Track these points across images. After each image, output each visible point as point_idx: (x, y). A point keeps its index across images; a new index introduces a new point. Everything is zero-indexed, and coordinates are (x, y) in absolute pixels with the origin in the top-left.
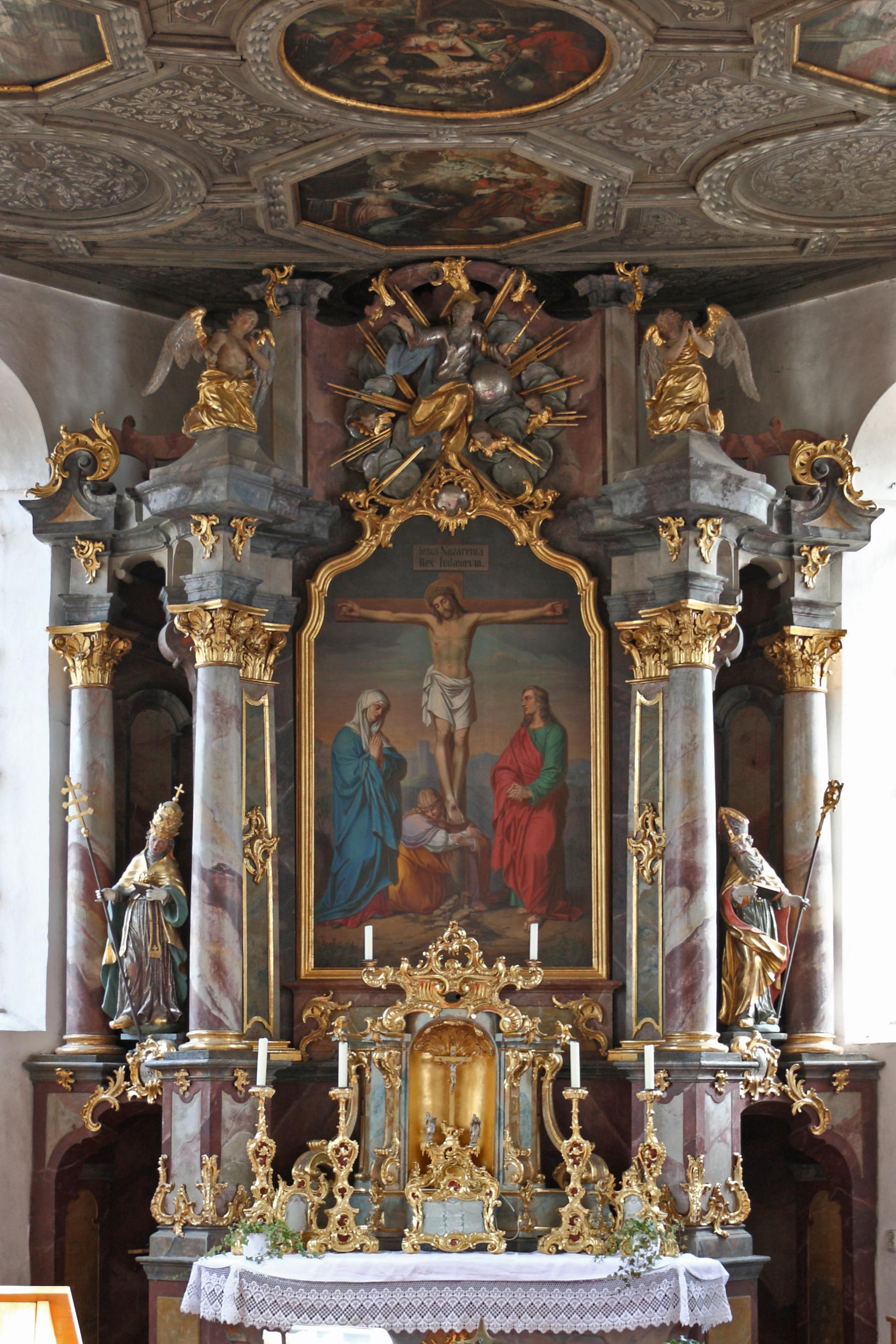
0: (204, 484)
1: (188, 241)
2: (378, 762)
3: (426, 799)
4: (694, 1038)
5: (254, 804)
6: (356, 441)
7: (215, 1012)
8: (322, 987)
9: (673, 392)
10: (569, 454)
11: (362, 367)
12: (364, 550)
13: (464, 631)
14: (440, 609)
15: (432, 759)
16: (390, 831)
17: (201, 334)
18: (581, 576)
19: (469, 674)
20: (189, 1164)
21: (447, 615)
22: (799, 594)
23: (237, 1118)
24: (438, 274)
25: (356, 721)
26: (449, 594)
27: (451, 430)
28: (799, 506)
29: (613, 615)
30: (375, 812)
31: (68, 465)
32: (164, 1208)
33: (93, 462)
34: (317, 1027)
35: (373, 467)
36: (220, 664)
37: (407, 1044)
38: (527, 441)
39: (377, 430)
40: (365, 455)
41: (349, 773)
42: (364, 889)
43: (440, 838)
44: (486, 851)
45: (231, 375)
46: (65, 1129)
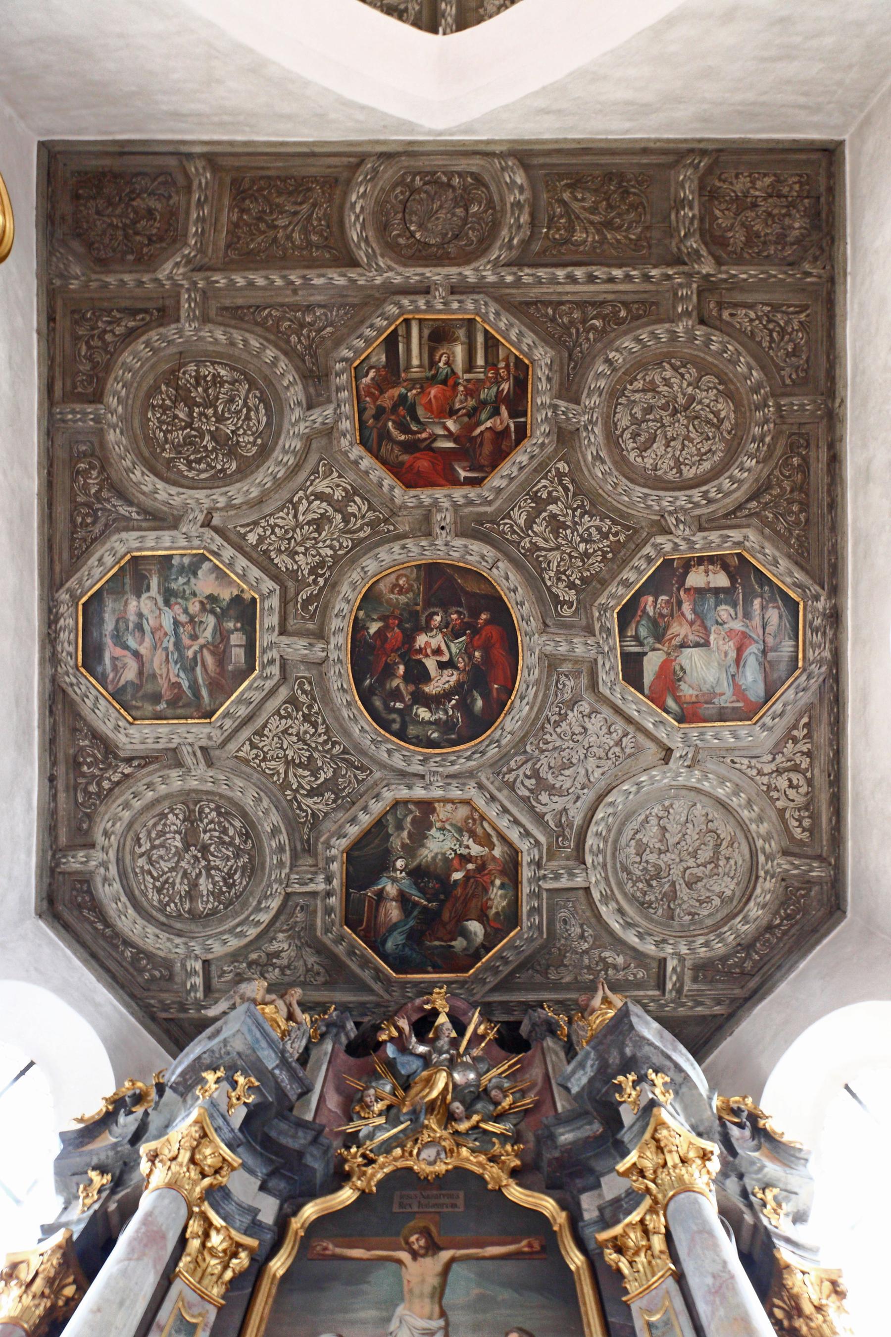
13: (439, 1268)
26: (425, 1232)
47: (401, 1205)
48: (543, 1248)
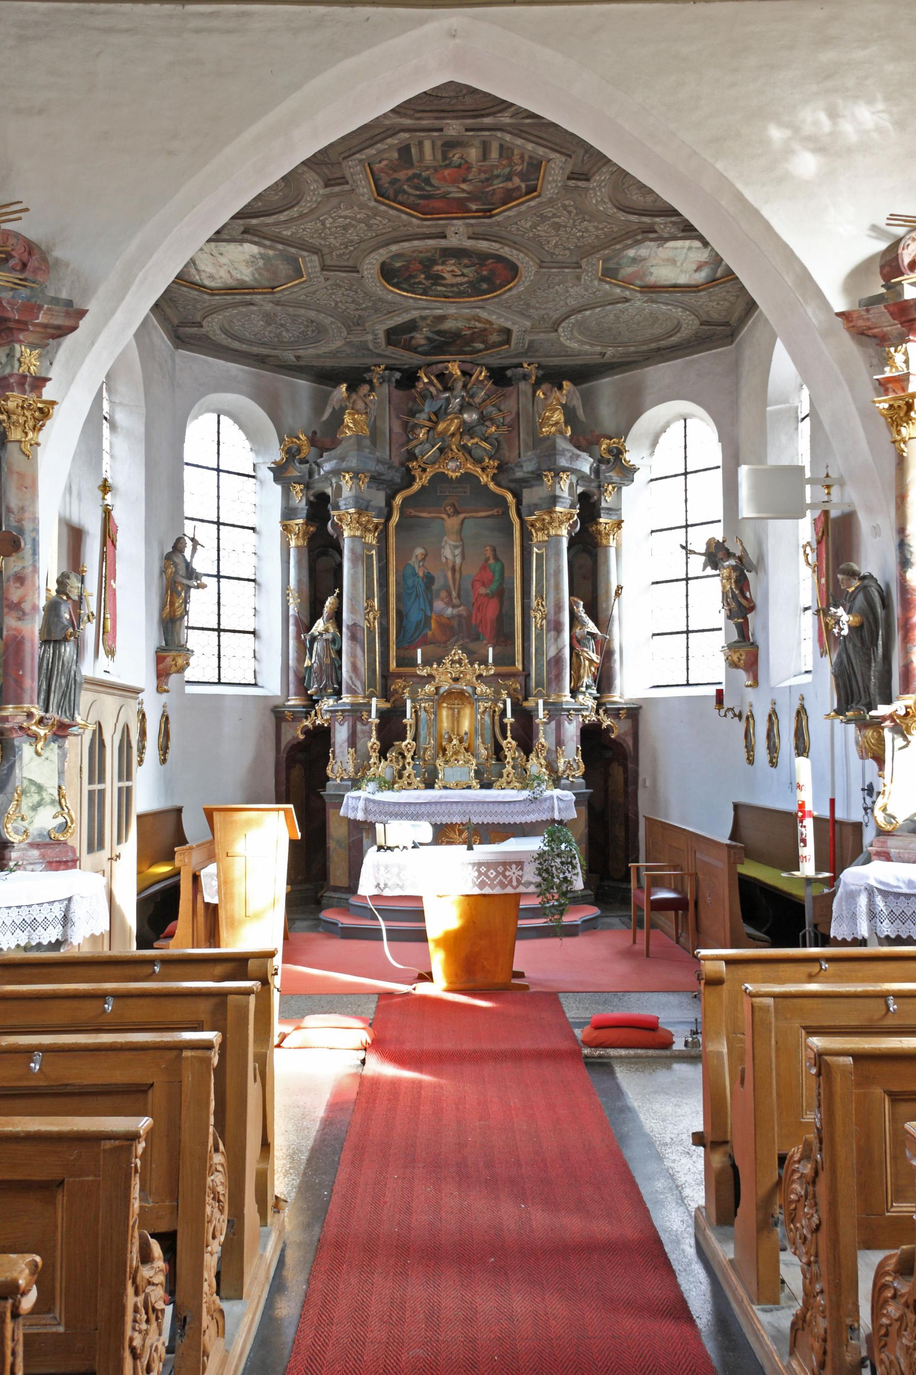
2: (423, 578)
3: (443, 594)
4: (560, 696)
5: (370, 597)
6: (412, 440)
8: (399, 676)
9: (549, 418)
10: (504, 445)
12: (416, 487)
13: (459, 522)
15: (446, 577)
16: (428, 608)
18: (510, 497)
22: (603, 505)
23: (363, 732)
24: (447, 368)
25: (413, 561)
26: (453, 505)
27: (453, 435)
28: (603, 467)
29: (523, 514)
30: (422, 600)
31: (288, 452)
33: (299, 450)
34: (397, 693)
36: (354, 536)
38: (486, 440)
40: (416, 446)
41: (410, 582)
43: (449, 611)
44: (469, 616)
45: (358, 412)
46: (289, 737)
47: (441, 492)
48: (503, 512)
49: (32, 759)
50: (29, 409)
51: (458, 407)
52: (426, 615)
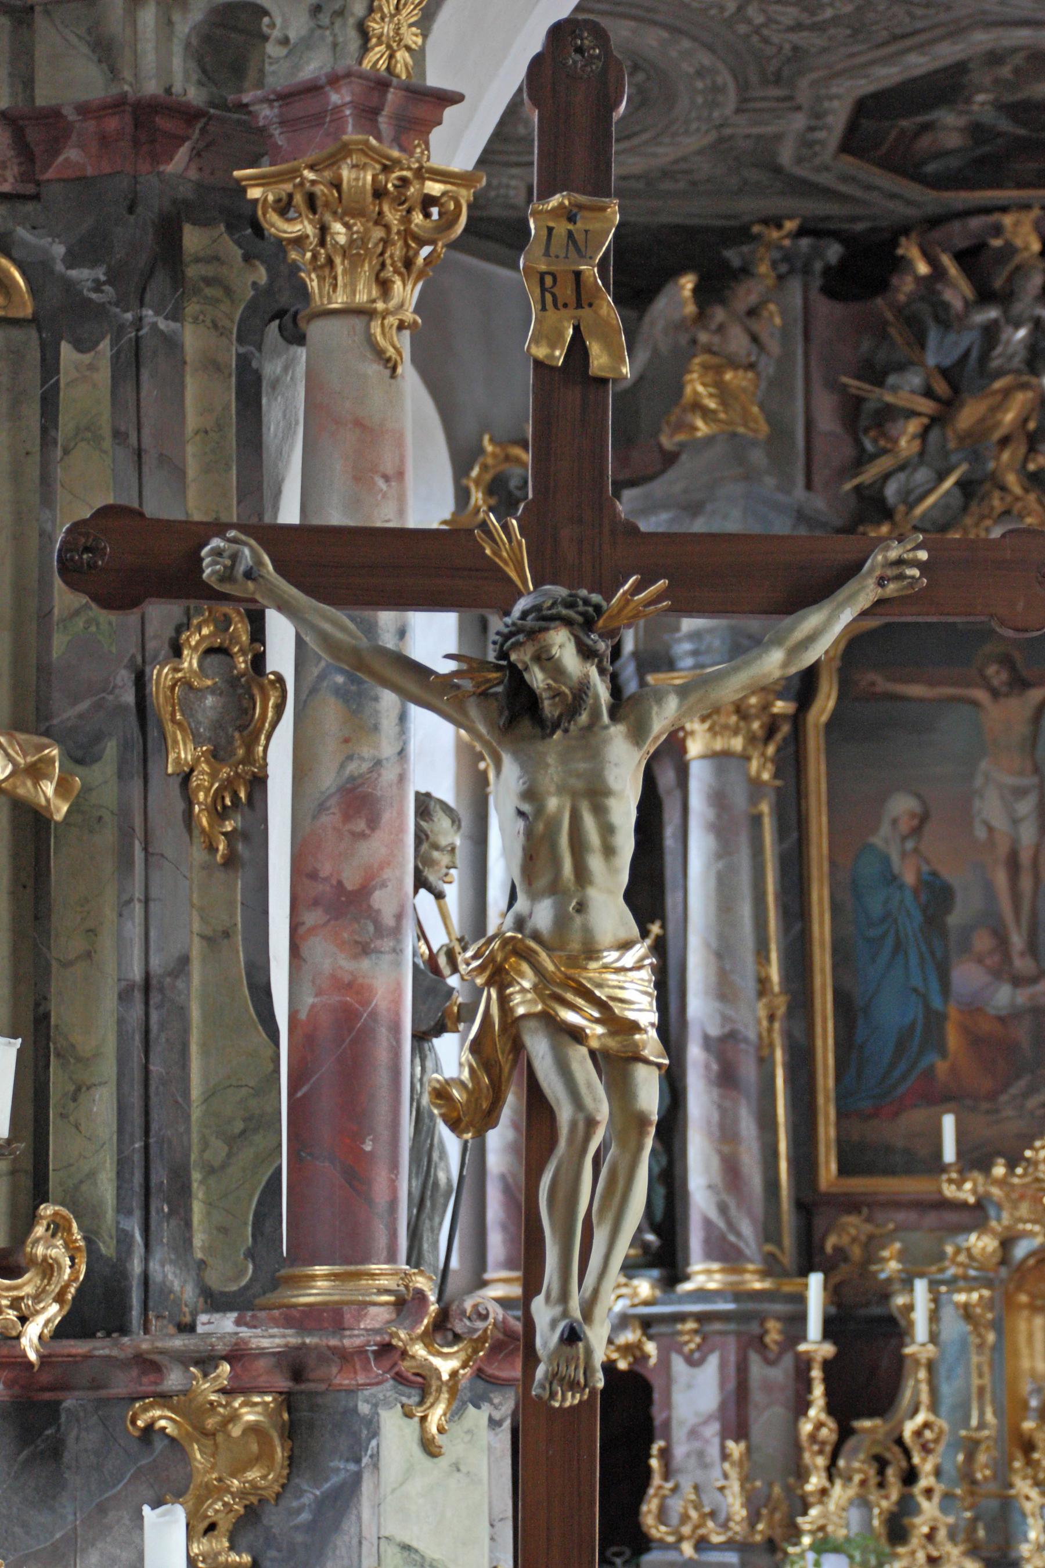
0: (709, 507)
1: (667, 185)
2: (916, 892)
3: (982, 942)
6: (873, 457)
7: (732, 1238)
8: (852, 1204)
11: (882, 356)
13: (1028, 712)
14: (995, 682)
15: (989, 887)
16: (934, 985)
17: (691, 309)
19: (1036, 770)
20: (701, 1454)
21: (1004, 689)
24: (998, 230)
25: (883, 838)
26: (1007, 661)
27: (1005, 442)
30: (914, 960)
32: (662, 1516)
34: (846, 1259)
35: (899, 492)
37: (1002, 1281)
39: (903, 442)
40: (886, 477)
41: (875, 906)
42: (903, 1066)
43: (1004, 996)
45: (733, 364)
49: (409, 1472)
50: (400, 200)
51: (1022, 354)
52: (927, 1007)
